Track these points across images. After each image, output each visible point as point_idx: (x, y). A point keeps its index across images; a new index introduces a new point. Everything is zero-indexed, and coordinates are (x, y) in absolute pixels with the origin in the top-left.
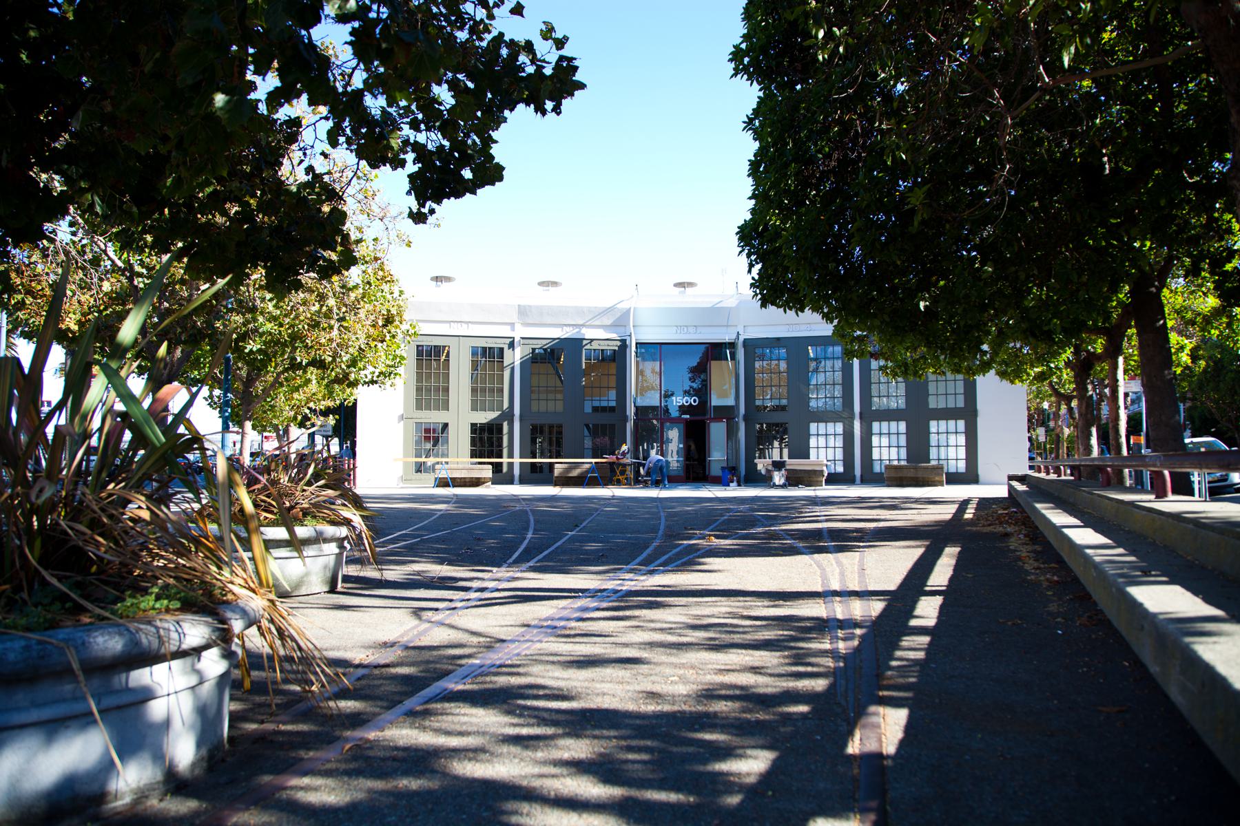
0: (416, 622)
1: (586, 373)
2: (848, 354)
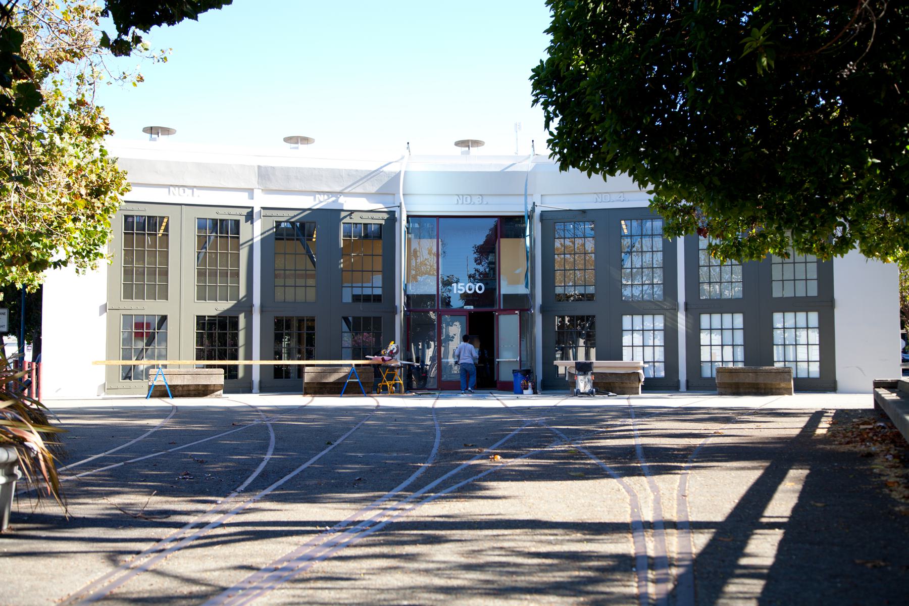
0: (110, 569)
1: (345, 253)
2: (672, 230)
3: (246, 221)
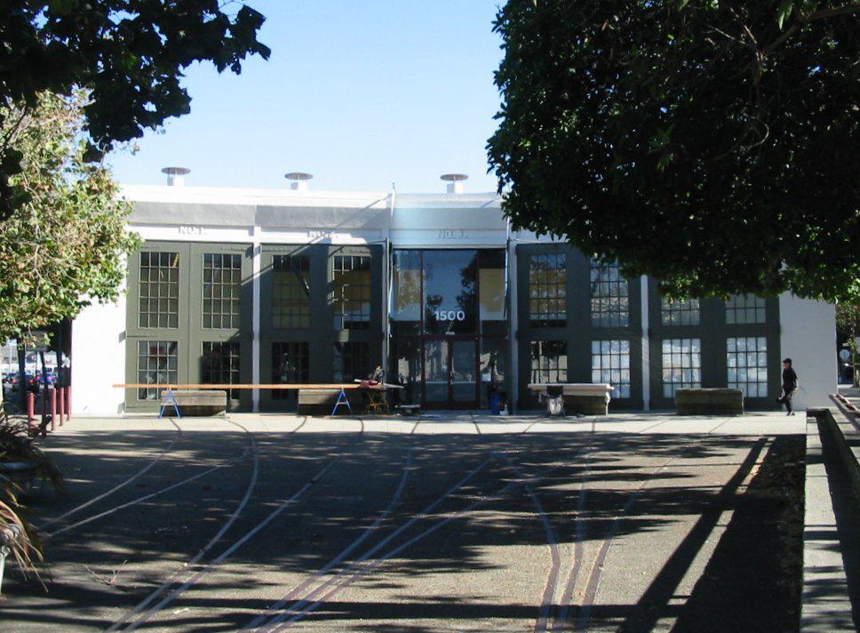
3: (247, 256)
